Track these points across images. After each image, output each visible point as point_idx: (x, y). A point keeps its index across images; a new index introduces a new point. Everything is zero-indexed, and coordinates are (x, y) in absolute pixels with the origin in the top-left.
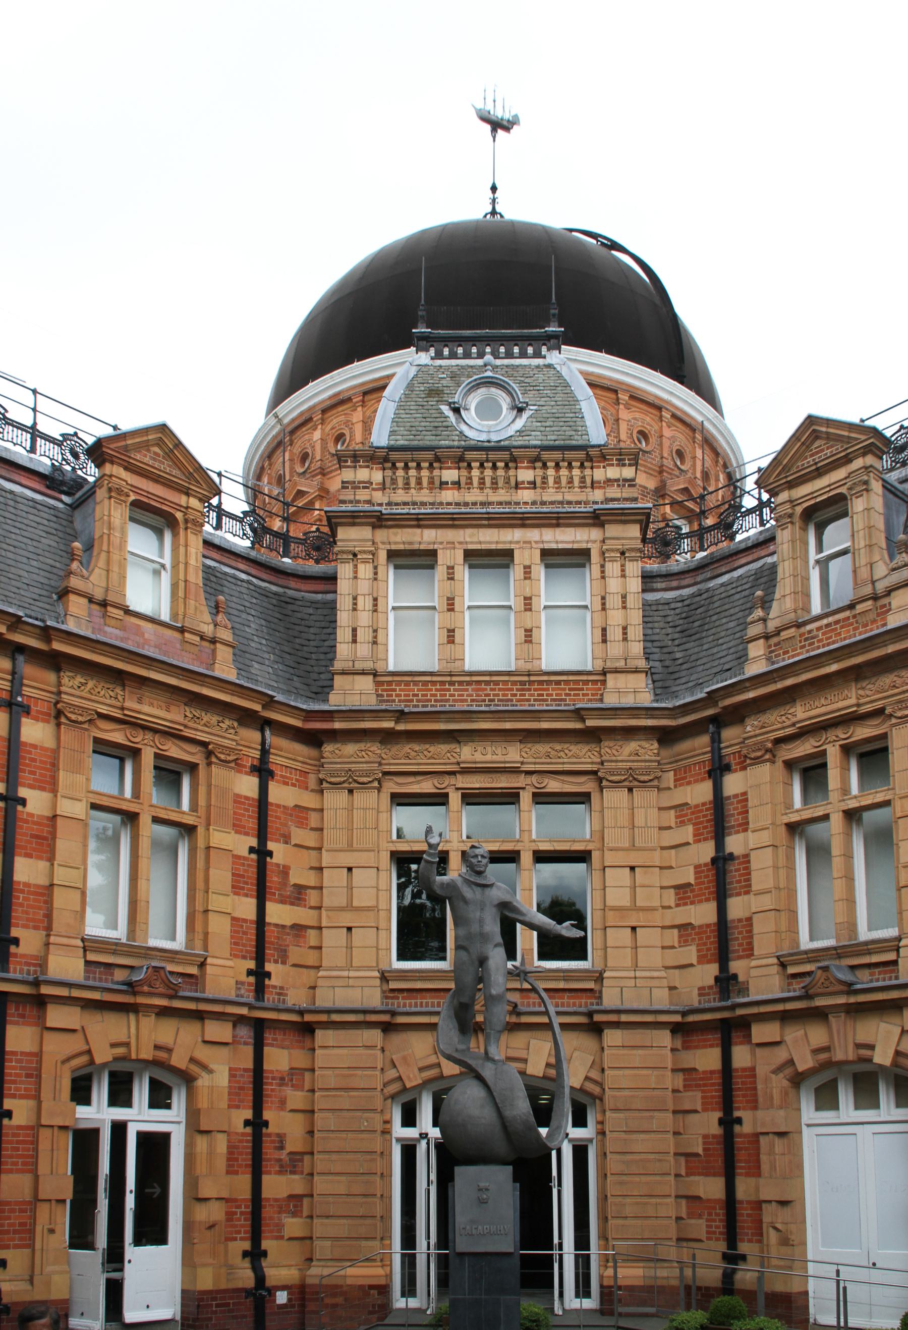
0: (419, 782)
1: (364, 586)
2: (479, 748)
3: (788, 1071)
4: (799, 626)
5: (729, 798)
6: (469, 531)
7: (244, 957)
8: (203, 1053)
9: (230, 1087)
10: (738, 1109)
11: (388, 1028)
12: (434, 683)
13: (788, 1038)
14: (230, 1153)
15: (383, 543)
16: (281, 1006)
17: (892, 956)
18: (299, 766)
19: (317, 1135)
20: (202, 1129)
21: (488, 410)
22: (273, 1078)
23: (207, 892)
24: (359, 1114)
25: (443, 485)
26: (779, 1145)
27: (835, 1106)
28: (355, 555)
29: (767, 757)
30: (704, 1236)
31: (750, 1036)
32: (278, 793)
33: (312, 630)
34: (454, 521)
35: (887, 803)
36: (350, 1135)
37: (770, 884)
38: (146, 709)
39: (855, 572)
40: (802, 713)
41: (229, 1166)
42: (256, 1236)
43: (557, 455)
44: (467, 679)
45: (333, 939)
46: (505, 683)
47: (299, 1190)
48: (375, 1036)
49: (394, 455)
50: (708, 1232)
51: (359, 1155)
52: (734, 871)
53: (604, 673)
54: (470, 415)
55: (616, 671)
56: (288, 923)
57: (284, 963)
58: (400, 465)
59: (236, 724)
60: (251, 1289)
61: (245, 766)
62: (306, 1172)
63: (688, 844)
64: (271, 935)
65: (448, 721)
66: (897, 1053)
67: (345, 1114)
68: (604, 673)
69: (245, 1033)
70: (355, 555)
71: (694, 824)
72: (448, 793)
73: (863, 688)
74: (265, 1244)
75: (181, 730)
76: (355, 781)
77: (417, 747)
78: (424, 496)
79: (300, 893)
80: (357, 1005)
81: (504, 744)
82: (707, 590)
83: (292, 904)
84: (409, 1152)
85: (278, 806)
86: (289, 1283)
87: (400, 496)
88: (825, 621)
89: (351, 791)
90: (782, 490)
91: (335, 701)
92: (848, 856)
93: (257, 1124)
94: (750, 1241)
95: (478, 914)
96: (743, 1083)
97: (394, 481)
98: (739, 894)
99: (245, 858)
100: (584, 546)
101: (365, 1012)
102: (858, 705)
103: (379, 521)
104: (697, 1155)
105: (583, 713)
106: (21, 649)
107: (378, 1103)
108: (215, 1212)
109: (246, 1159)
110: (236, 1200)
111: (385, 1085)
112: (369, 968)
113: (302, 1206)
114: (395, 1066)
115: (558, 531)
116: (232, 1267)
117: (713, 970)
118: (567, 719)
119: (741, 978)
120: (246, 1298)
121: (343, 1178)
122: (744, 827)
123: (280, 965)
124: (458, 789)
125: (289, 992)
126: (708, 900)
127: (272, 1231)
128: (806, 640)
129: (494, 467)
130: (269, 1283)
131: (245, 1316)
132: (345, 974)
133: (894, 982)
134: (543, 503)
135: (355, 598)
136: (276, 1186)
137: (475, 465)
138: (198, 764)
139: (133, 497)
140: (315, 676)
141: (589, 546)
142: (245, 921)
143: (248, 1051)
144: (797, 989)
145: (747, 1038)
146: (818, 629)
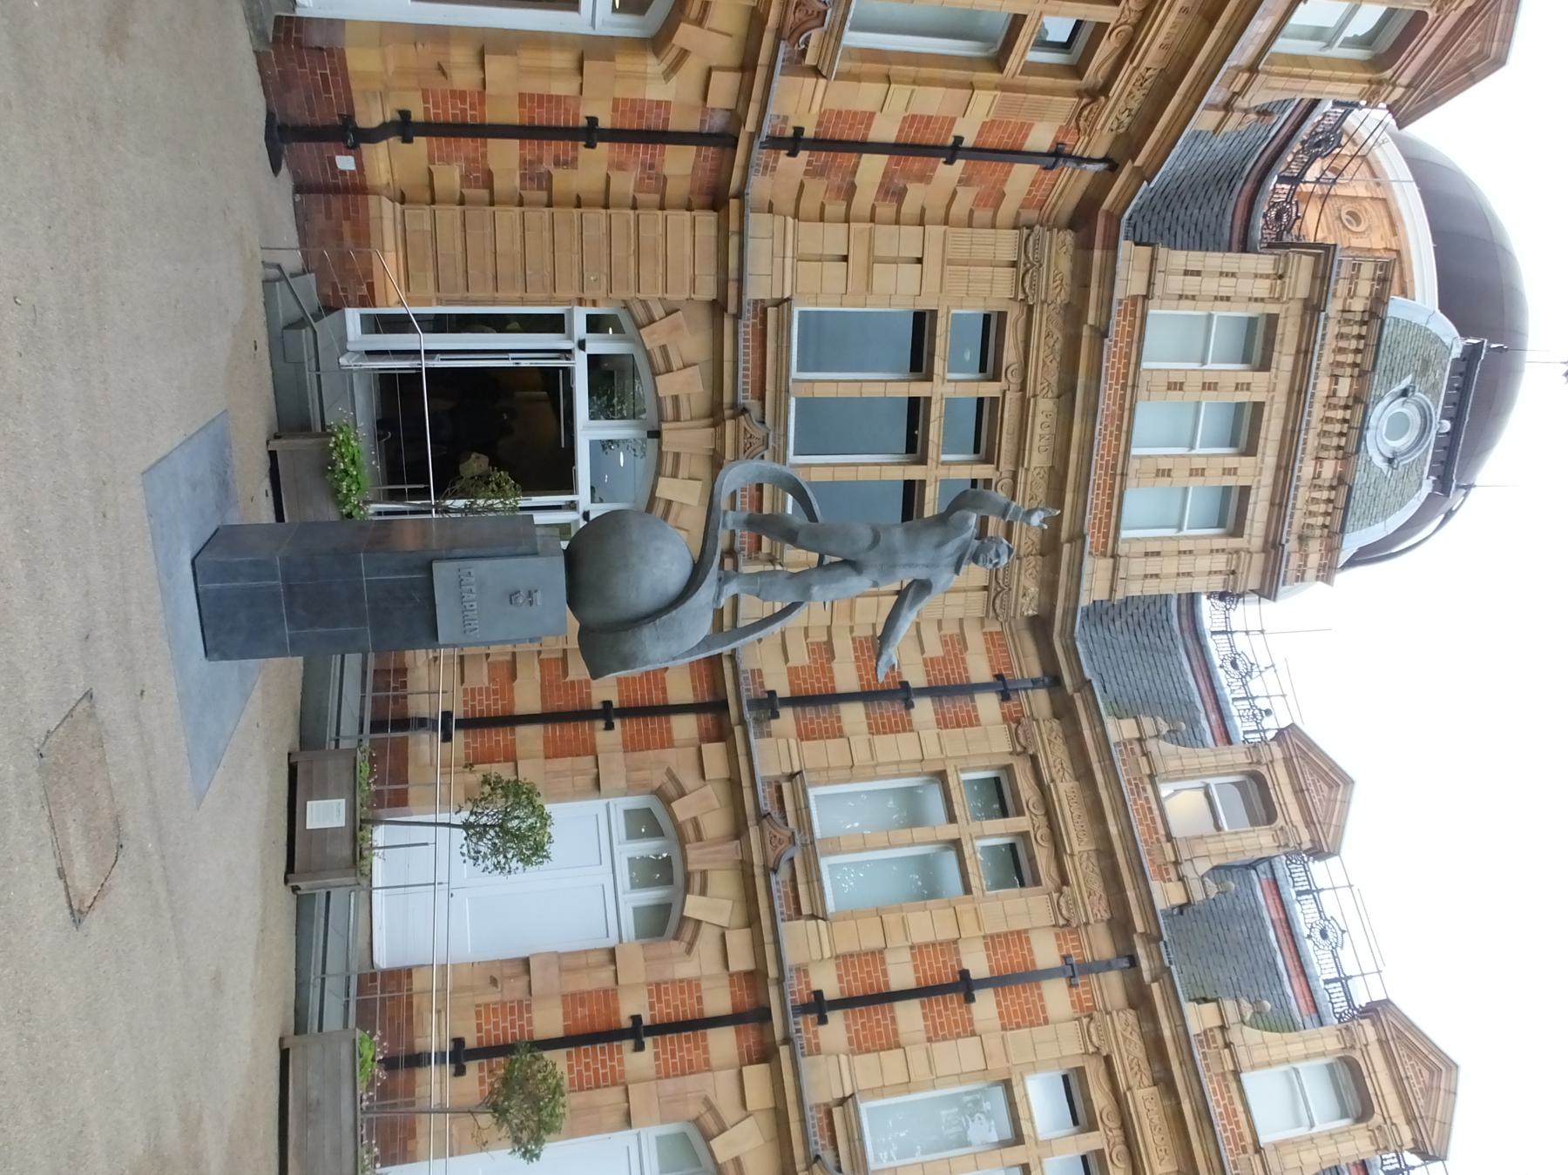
0: (1016, 346)
3: (671, 790)
4: (1152, 777)
5: (973, 700)
6: (1283, 407)
7: (820, 124)
8: (707, 944)
9: (643, 101)
10: (623, 725)
11: (717, 307)
12: (1127, 365)
13: (709, 789)
14: (550, 97)
17: (806, 910)
19: (576, 212)
20: (586, 63)
21: (1398, 426)
22: (653, 156)
24: (606, 269)
25: (1335, 378)
26: (585, 780)
27: (633, 835)
28: (1281, 277)
29: (1019, 749)
32: (1022, 175)
34: (1298, 393)
35: (967, 889)
36: (576, 258)
38: (1172, 18)
39: (1202, 837)
40: (1065, 788)
41: (532, 96)
42: (432, 129)
43: (1341, 503)
44: (1127, 405)
45: (833, 237)
46: (1117, 448)
48: (707, 291)
49: (1376, 324)
50: (473, 690)
51: (549, 269)
52: (892, 709)
53: (1114, 556)
54: (1397, 407)
55: (1115, 569)
56: (857, 180)
57: (806, 173)
58: (1364, 330)
59: (1122, 130)
61: (1065, 136)
63: (923, 652)
64: (845, 159)
66: (699, 922)
67: (605, 251)
68: (1114, 556)
69: (717, 123)
70: (1281, 277)
74: (421, 142)
76: (1027, 271)
77: (1057, 346)
78: (1328, 357)
79: (894, 194)
80: (749, 268)
81: (1051, 449)
82: (1176, 647)
83: (881, 185)
84: (555, 324)
86: (367, 172)
88: (1154, 806)
89: (1014, 264)
91: (1125, 247)
92: (912, 844)
93: (591, 133)
94: (467, 746)
95: (921, 562)
96: (653, 730)
97: (1347, 322)
99: (950, 130)
100: (1247, 531)
101: (740, 280)
103: (1313, 308)
104: (566, 674)
106: (1133, 961)
107: (620, 294)
108: (464, 77)
109: (541, 117)
111: (644, 303)
112: (794, 286)
114: (668, 314)
115: (1267, 504)
116: (383, 96)
117: (783, 691)
121: (518, 247)
122: (943, 722)
124: (1004, 393)
127: (439, 148)
129: (1341, 434)
131: (312, 113)
132: (789, 253)
133: (779, 918)
135: (1233, 275)
136: (505, 157)
137: (1348, 414)
139: (1432, 14)
142: (868, 127)
143: (692, 124)
144: (767, 804)
146: (1147, 799)
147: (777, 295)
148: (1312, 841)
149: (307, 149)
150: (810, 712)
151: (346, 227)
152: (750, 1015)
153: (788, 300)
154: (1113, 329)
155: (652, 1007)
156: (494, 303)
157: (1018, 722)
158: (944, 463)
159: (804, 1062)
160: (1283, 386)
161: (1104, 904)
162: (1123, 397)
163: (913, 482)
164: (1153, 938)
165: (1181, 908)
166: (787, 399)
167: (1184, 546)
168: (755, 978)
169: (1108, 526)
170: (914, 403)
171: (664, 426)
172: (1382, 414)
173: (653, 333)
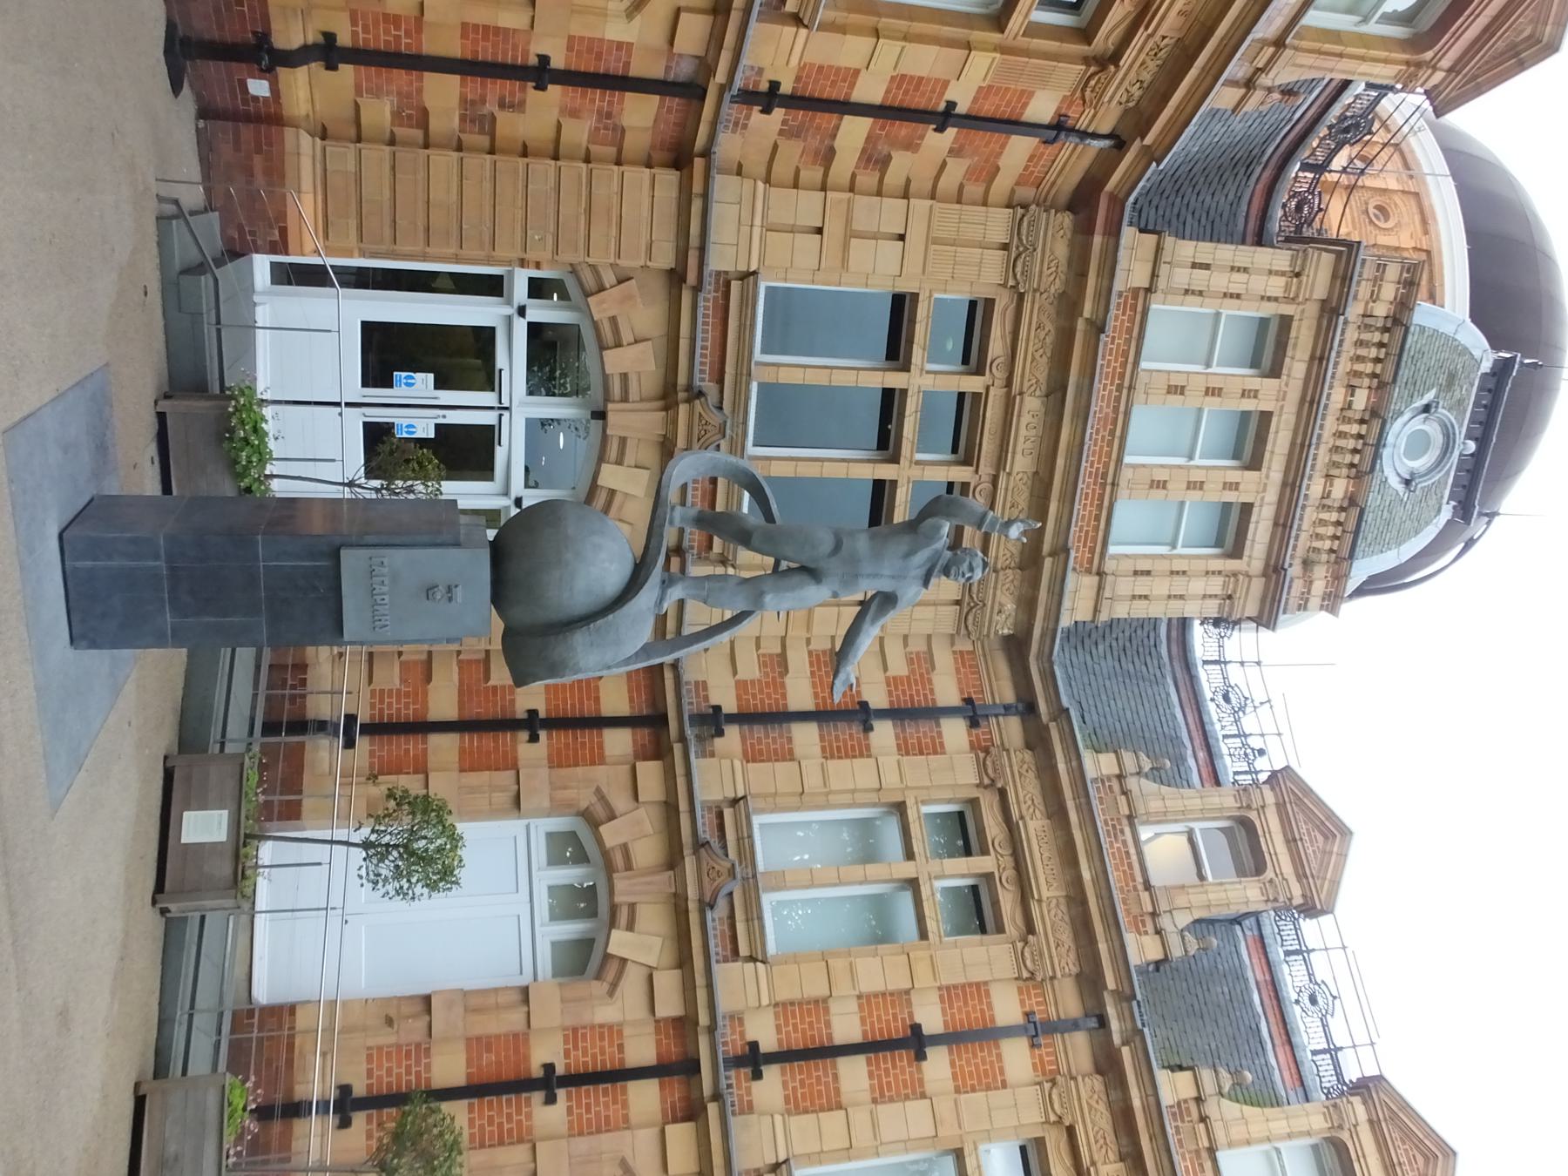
0: (1003, 337)
1: (1259, 284)
2: (1035, 420)
3: (600, 811)
4: (1130, 818)
5: (938, 725)
6: (1293, 419)
8: (633, 983)
9: (601, 40)
10: (550, 737)
11: (675, 277)
12: (1124, 365)
13: (642, 812)
14: (497, 30)
15: (1303, 311)
16: (720, 127)
17: (744, 950)
18: (1051, 177)
19: (522, 161)
21: (1418, 444)
22: (610, 103)
23: (905, 39)
24: (552, 228)
25: (1352, 389)
26: (503, 798)
27: (555, 860)
28: (1298, 275)
29: (986, 781)
30: (376, 686)
31: (645, 759)
32: (1020, 148)
33: (1209, 198)
34: (1311, 402)
35: (923, 935)
36: (520, 214)
37: (835, 784)
40: (1035, 827)
41: (476, 26)
42: (359, 56)
43: (1351, 526)
44: (1122, 409)
45: (807, 206)
46: (1109, 455)
47: (435, 124)
48: (665, 258)
49: (1399, 332)
50: (382, 691)
51: (489, 224)
52: (848, 732)
54: (1418, 424)
55: (1100, 588)
56: (837, 144)
57: (781, 133)
59: (1131, 105)
60: (269, 43)
61: (1069, 107)
62: (463, 137)
64: (824, 120)
65: (1079, 388)
66: (624, 961)
70: (1298, 275)
71: (908, 678)
72: (983, 374)
73: (1058, 905)
75: (1147, 28)
76: (1019, 256)
77: (1048, 340)
78: (1345, 366)
79: (876, 162)
80: (713, 236)
82: (1164, 676)
83: (864, 151)
84: (492, 286)
85: (1003, 146)
87: (1352, 335)
88: (1132, 851)
90: (1276, 796)
91: (1128, 233)
93: (541, 74)
96: (583, 744)
98: (822, 738)
101: (702, 249)
102: (1040, 901)
103: (1331, 311)
105: (1062, 557)
106: (1103, 1022)
107: (567, 257)
109: (486, 52)
110: (419, 30)
111: (593, 267)
113: (411, 126)
114: (620, 282)
115: (1270, 523)
117: (730, 707)
118: (1057, 533)
119: (717, 741)
120: (255, 33)
121: (454, 196)
122: (904, 749)
123: (779, 126)
124: (988, 388)
125: (737, 136)
126: (816, 695)
128: (1114, 826)
129: (1355, 451)
130: (282, 72)
131: (221, 27)
132: (758, 221)
134: (1304, 507)
135: (1246, 270)
138: (1090, 44)
140: (1154, 203)
141: (1245, 558)
143: (656, 71)
144: (706, 832)
145: (642, 754)
146: (1124, 842)
147: (742, 268)
148: (1304, 896)
149: (214, 70)
150: (758, 731)
151: (258, 161)
152: (677, 1068)
153: (755, 273)
154: (1111, 324)
155: (567, 1054)
156: (424, 258)
157: (987, 751)
158: (918, 463)
159: (734, 1122)
160: (1294, 395)
161: (1072, 955)
162: (1118, 399)
163: (883, 482)
164: (1126, 997)
165: (1158, 964)
166: (748, 384)
167: (1178, 565)
168: (684, 1025)
169: (1094, 540)
170: (888, 395)
171: (610, 406)
172: (1402, 430)
173: (602, 302)
